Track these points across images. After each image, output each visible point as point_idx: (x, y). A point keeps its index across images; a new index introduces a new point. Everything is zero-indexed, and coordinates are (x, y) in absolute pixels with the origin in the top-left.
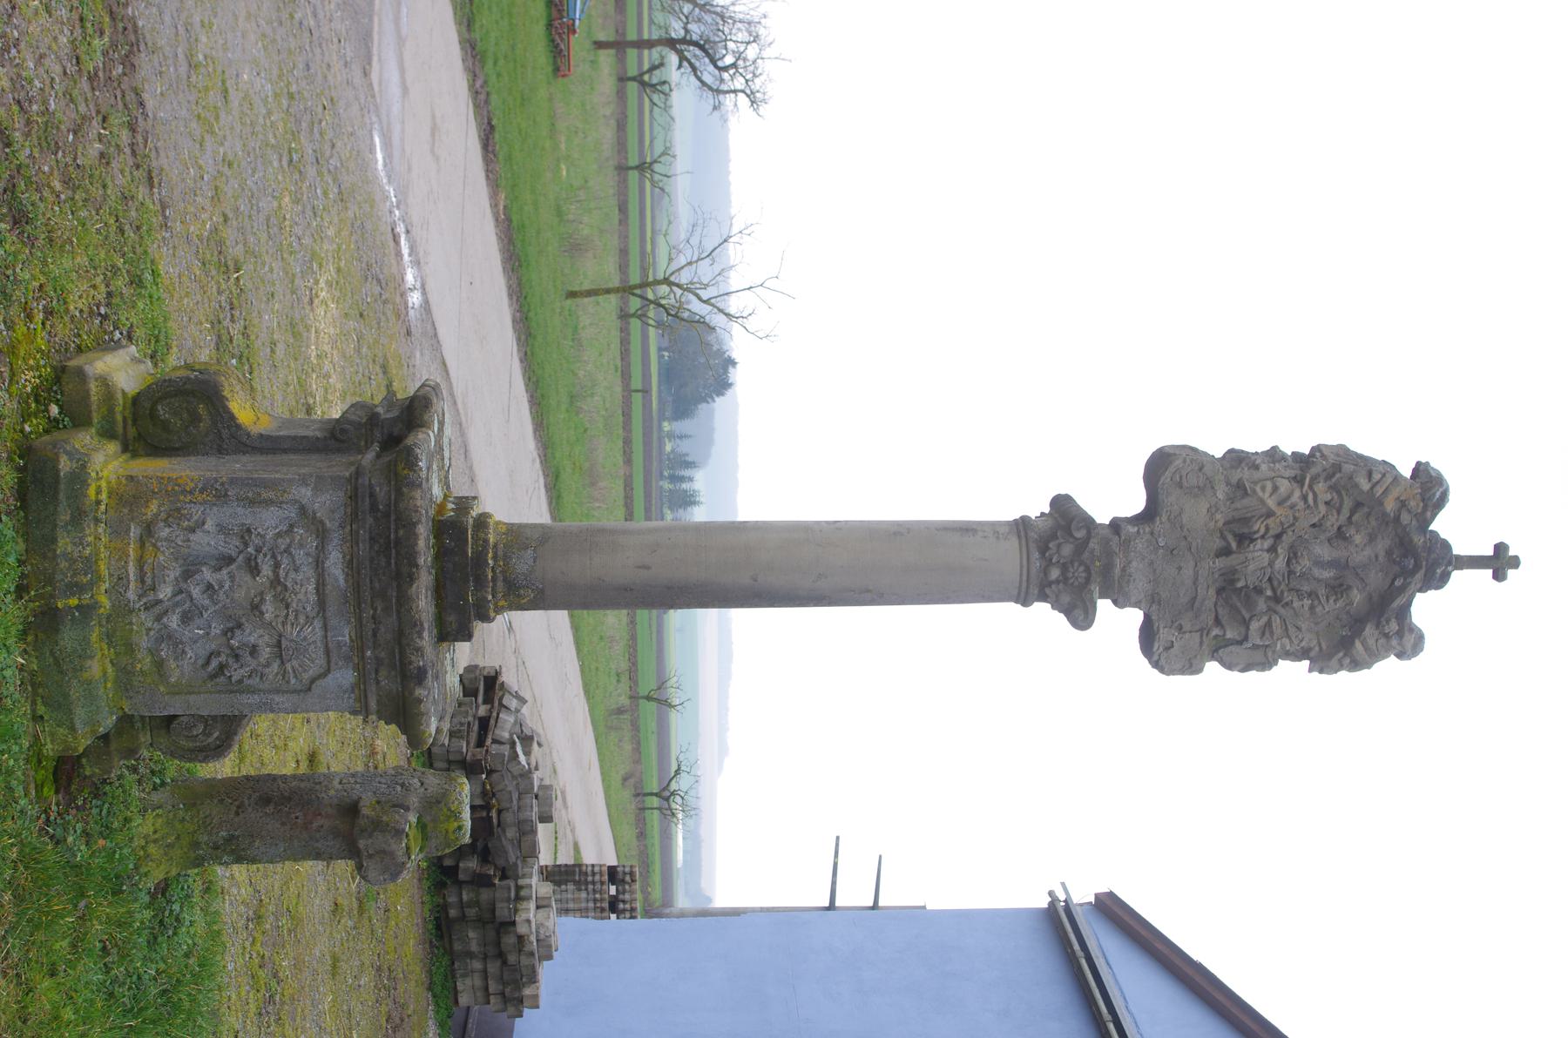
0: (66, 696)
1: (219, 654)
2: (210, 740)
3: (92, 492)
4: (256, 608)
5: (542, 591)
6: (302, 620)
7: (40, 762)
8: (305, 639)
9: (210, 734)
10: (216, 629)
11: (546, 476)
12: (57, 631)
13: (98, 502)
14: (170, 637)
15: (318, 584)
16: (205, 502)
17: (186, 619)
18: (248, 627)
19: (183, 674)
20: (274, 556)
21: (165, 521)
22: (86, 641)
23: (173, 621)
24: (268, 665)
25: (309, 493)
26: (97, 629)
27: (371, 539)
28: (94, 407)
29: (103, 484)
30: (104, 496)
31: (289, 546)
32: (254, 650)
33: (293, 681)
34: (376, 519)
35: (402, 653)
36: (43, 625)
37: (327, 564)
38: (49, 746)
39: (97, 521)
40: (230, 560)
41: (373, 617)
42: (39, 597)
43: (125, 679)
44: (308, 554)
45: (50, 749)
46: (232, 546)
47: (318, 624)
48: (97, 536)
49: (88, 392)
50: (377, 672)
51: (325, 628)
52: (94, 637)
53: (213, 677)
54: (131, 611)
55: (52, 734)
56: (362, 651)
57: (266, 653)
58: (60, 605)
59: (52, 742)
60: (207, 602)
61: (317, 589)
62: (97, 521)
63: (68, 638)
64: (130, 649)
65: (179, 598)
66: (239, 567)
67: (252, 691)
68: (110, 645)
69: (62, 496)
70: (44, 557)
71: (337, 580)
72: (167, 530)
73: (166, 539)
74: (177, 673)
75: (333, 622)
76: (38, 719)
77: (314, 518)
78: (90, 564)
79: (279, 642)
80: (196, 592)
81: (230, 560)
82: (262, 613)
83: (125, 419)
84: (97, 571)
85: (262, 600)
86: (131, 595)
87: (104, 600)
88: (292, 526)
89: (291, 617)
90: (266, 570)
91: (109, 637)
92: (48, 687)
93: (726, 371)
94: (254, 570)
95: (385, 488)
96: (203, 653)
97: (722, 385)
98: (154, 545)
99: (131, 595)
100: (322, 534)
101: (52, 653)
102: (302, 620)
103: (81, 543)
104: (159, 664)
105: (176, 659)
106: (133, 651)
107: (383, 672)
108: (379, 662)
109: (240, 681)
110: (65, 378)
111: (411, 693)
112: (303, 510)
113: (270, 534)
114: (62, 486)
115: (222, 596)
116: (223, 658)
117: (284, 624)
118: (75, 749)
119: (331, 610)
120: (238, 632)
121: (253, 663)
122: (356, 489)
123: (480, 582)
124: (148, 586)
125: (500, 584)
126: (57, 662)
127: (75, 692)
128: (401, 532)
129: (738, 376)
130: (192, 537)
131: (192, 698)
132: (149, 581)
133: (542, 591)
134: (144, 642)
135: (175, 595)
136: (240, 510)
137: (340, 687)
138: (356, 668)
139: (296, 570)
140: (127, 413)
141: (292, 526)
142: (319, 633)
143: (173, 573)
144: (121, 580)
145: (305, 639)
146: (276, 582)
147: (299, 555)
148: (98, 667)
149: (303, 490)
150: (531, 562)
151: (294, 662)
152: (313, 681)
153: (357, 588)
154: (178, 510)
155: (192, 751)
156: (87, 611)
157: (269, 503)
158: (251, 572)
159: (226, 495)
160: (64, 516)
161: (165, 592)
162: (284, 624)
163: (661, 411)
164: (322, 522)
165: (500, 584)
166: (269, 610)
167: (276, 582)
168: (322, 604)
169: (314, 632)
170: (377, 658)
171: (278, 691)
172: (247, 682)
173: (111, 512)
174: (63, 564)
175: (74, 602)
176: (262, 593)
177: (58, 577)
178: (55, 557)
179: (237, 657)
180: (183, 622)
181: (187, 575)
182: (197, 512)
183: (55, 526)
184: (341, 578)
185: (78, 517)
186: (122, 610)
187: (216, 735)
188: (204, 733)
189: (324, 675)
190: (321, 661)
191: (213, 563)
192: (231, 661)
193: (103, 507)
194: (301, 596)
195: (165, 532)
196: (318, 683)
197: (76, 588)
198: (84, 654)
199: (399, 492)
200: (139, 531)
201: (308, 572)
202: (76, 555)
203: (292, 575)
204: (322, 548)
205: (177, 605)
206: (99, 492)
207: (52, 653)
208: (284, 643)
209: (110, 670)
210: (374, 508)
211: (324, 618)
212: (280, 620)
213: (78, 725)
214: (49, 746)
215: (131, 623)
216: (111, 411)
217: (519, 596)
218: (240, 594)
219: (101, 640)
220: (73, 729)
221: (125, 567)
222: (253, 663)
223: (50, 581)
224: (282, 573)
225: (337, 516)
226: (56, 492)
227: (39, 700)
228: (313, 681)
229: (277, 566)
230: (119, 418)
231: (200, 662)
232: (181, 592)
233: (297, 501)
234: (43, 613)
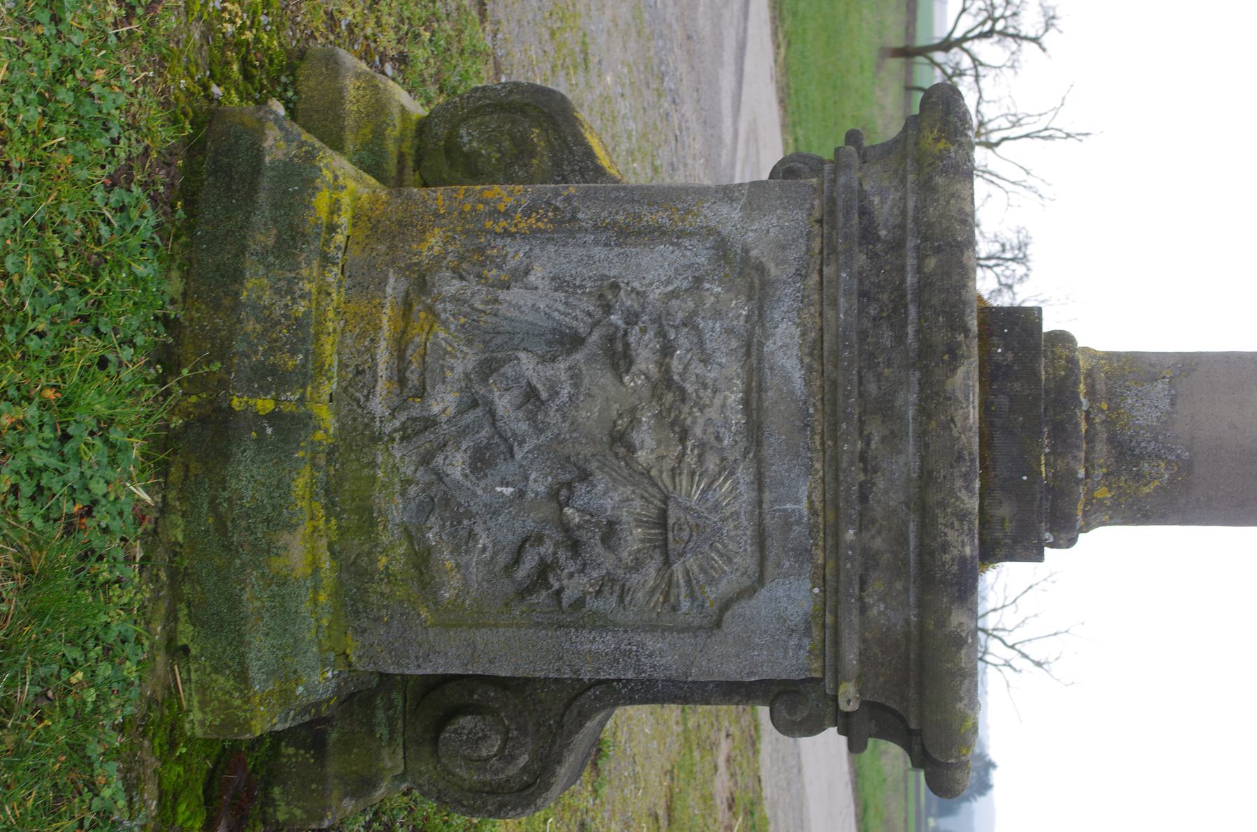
0: (234, 603)
1: (540, 540)
2: (512, 771)
3: (322, 202)
4: (620, 440)
5: (1187, 467)
6: (712, 463)
7: (173, 745)
8: (716, 507)
9: (512, 758)
10: (539, 484)
11: (857, 805)
12: (226, 457)
13: (332, 228)
14: (447, 501)
15: (747, 392)
16: (534, 232)
17: (481, 462)
18: (601, 482)
19: (466, 583)
20: (662, 334)
21: (454, 270)
22: (282, 488)
23: (456, 465)
24: (637, 565)
25: (736, 215)
26: (306, 470)
27: (863, 294)
28: (349, 122)
29: (346, 199)
30: (344, 219)
31: (694, 313)
32: (610, 532)
33: (685, 605)
34: (873, 256)
35: (927, 526)
36: (196, 445)
37: (770, 346)
38: (196, 715)
39: (326, 260)
40: (573, 341)
41: (863, 458)
42: (197, 383)
43: (355, 584)
44: (729, 331)
45: (196, 721)
46: (577, 313)
47: (744, 474)
48: (321, 289)
49: (341, 91)
50: (863, 584)
51: (759, 484)
52: (300, 484)
53: (524, 592)
54: (376, 439)
55: (203, 689)
56: (835, 532)
57: (634, 538)
58: (235, 402)
59: (203, 704)
60: (523, 426)
61: (746, 402)
62: (326, 260)
63: (247, 476)
64: (368, 520)
65: (470, 416)
66: (591, 359)
67: (602, 624)
68: (330, 508)
69: (262, 197)
70: (217, 307)
71: (787, 379)
72: (457, 284)
73: (455, 299)
74: (456, 580)
75: (777, 469)
76: (178, 652)
77: (746, 259)
78: (303, 333)
79: (663, 514)
80: (504, 403)
81: (573, 341)
82: (631, 449)
83: (401, 156)
84: (318, 355)
85: (634, 422)
86: (378, 406)
87: (325, 414)
88: (698, 280)
89: (691, 459)
90: (645, 360)
91: (330, 492)
92: (201, 582)
93: (987, 773)
94: (619, 358)
95: (893, 196)
96: (510, 538)
97: (984, 787)
98: (430, 309)
99: (378, 406)
100: (759, 290)
101: (214, 506)
102: (712, 463)
103: (289, 290)
104: (422, 560)
105: (456, 550)
106: (372, 524)
107: (877, 586)
108: (869, 560)
109: (579, 603)
110: (304, 70)
111: (942, 623)
112: (722, 249)
113: (655, 294)
114: (265, 183)
115: (554, 417)
116: (547, 549)
117: (674, 473)
118: (245, 725)
119: (774, 442)
120: (581, 488)
121: (609, 562)
122: (832, 201)
123: (1062, 434)
124: (410, 389)
125: (1101, 447)
126: (220, 519)
127: (253, 599)
128: (931, 263)
129: (996, 777)
130: (503, 295)
131: (481, 637)
132: (413, 378)
133: (1187, 467)
134: (396, 511)
135: (461, 412)
136: (599, 252)
137: (782, 619)
138: (821, 579)
139: (706, 361)
140: (407, 147)
141: (698, 280)
142: (747, 495)
143: (463, 363)
144: (361, 375)
145: (716, 507)
146: (665, 383)
147: (712, 329)
148: (303, 550)
149: (724, 209)
150: (1165, 404)
151: (692, 562)
152: (726, 606)
153: (830, 395)
154: (481, 250)
155: (476, 791)
156: (289, 426)
157: (657, 234)
158: (615, 367)
159: (574, 218)
160: (263, 237)
161: (443, 402)
162: (674, 473)
163: (928, 807)
164: (760, 269)
165: (1101, 447)
166: (648, 444)
167: (665, 383)
168: (754, 431)
169: (733, 494)
170: (865, 552)
171: (652, 628)
172: (593, 604)
173: (355, 251)
174: (251, 326)
175: (265, 404)
176: (633, 410)
177: (239, 346)
178: (237, 306)
179: (575, 547)
180: (474, 470)
181: (488, 368)
182: (515, 252)
183: (243, 249)
184: (797, 376)
185: (291, 240)
186: (359, 436)
187: (523, 760)
188: (500, 754)
189: (748, 592)
190: (746, 560)
191: (541, 349)
192: (562, 555)
193: (340, 238)
194: (712, 413)
195: (452, 287)
196: (736, 608)
197: (270, 378)
198: (278, 519)
199: (926, 187)
200: (403, 286)
201: (727, 368)
202: (277, 312)
203: (697, 368)
204: (759, 316)
205: (464, 432)
206: (335, 208)
207: (214, 506)
208: (673, 515)
209: (326, 564)
210: (868, 234)
211: (759, 461)
212: (669, 463)
213: (253, 672)
214: (196, 715)
215: (373, 465)
216: (379, 134)
217: (1138, 477)
218: (589, 414)
219: (314, 496)
220: (242, 677)
221: (371, 351)
222: (609, 562)
223: (222, 352)
224: (676, 366)
225: (792, 255)
226: (253, 189)
227: (183, 613)
228: (726, 606)
229: (667, 350)
230: (391, 147)
231: (502, 559)
232: (474, 404)
233: (711, 231)
234: (203, 420)
